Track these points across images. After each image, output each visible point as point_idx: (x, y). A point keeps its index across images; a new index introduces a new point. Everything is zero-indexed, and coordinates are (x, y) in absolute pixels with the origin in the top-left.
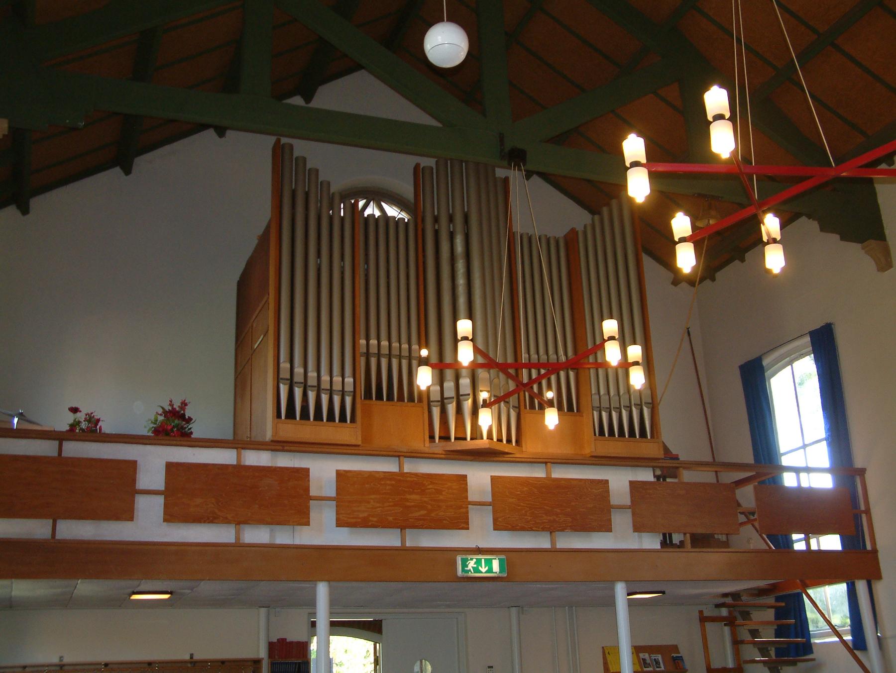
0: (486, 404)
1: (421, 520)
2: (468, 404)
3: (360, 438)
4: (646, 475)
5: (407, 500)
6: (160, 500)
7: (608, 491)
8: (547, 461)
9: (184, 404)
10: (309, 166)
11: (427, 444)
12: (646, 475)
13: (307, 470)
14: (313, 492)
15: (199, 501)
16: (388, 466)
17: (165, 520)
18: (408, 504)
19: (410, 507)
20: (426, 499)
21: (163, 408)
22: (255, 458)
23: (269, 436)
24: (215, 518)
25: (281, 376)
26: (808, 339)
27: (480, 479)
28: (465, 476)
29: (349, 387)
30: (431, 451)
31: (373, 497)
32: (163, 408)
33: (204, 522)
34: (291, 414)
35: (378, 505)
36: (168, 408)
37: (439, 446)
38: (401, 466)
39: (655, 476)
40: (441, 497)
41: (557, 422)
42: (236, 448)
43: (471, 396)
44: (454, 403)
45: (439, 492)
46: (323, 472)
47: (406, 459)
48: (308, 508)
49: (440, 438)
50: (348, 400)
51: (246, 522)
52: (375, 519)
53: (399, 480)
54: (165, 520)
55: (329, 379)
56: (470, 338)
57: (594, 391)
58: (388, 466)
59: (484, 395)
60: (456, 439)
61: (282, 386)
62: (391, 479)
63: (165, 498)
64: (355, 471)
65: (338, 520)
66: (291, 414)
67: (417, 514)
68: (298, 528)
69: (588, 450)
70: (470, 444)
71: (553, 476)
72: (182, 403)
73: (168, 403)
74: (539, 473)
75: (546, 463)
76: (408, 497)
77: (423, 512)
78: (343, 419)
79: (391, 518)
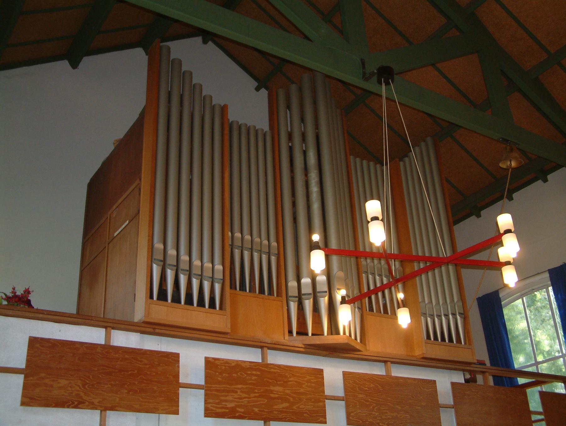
0: (344, 301)
1: (285, 412)
2: (324, 302)
3: (229, 326)
4: (459, 378)
5: (272, 392)
6: (19, 379)
7: (436, 391)
8: (385, 361)
9: (27, 292)
10: (184, 68)
11: (287, 337)
12: (459, 378)
13: (177, 356)
14: (182, 379)
15: (63, 382)
16: (250, 356)
17: (23, 404)
18: (272, 395)
19: (274, 398)
20: (288, 392)
21: (5, 294)
22: (124, 339)
23: (139, 316)
24: (80, 403)
25: (154, 257)
26: (547, 275)
27: (334, 373)
28: (322, 371)
29: (219, 276)
30: (291, 344)
31: (240, 386)
32: (5, 294)
33: (68, 407)
34: (162, 295)
35: (244, 395)
36: (11, 295)
37: (298, 341)
38: (264, 357)
39: (465, 380)
40: (302, 390)
41: (409, 321)
42: (106, 327)
43: (328, 293)
44: (312, 300)
45: (300, 385)
46: (193, 359)
47: (269, 351)
48: (177, 395)
49: (298, 333)
50: (217, 287)
51: (112, 409)
52: (242, 410)
53: (263, 371)
54: (23, 404)
55: (200, 264)
56: (380, 218)
57: (420, 300)
58: (250, 356)
59: (340, 293)
60: (313, 335)
61: (155, 266)
62: (256, 370)
63: (25, 377)
64: (223, 360)
65: (206, 409)
66: (162, 295)
67: (281, 406)
68: (163, 416)
69: (418, 352)
70: (327, 338)
71: (393, 375)
72: (25, 291)
73: (11, 290)
74: (378, 370)
75: (385, 362)
76: (272, 388)
77: (286, 405)
78: (212, 305)
79: (256, 410)
